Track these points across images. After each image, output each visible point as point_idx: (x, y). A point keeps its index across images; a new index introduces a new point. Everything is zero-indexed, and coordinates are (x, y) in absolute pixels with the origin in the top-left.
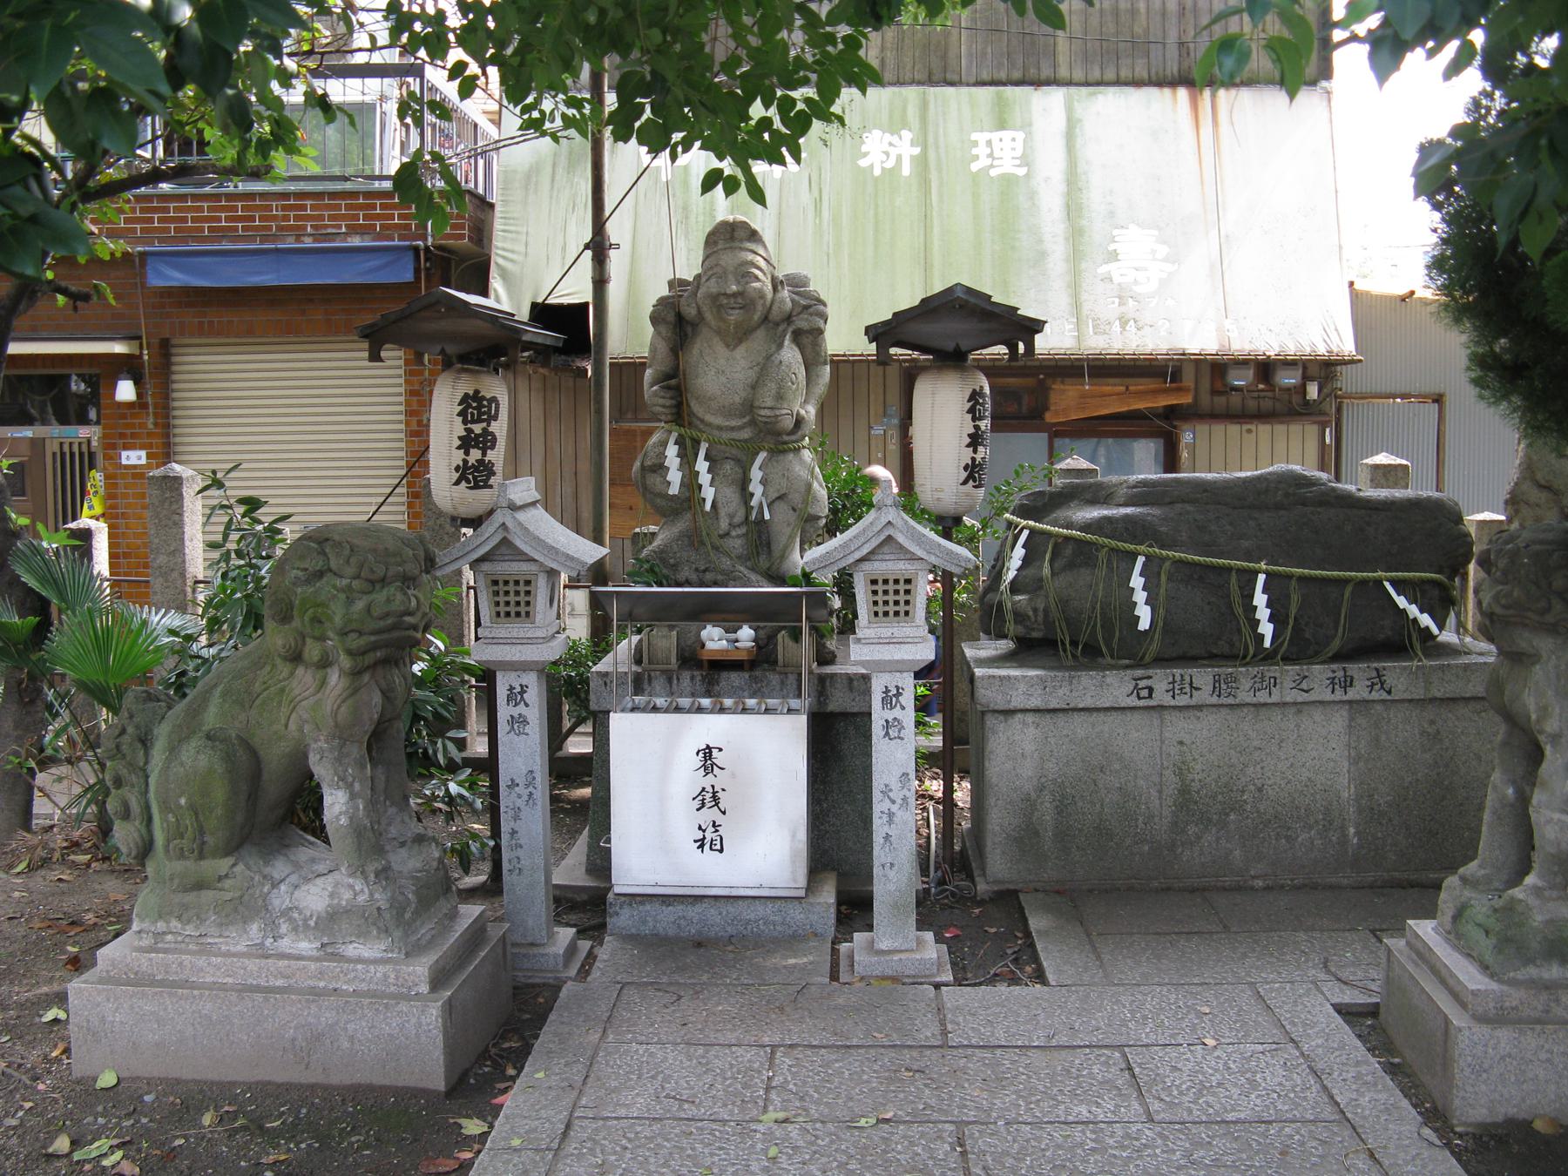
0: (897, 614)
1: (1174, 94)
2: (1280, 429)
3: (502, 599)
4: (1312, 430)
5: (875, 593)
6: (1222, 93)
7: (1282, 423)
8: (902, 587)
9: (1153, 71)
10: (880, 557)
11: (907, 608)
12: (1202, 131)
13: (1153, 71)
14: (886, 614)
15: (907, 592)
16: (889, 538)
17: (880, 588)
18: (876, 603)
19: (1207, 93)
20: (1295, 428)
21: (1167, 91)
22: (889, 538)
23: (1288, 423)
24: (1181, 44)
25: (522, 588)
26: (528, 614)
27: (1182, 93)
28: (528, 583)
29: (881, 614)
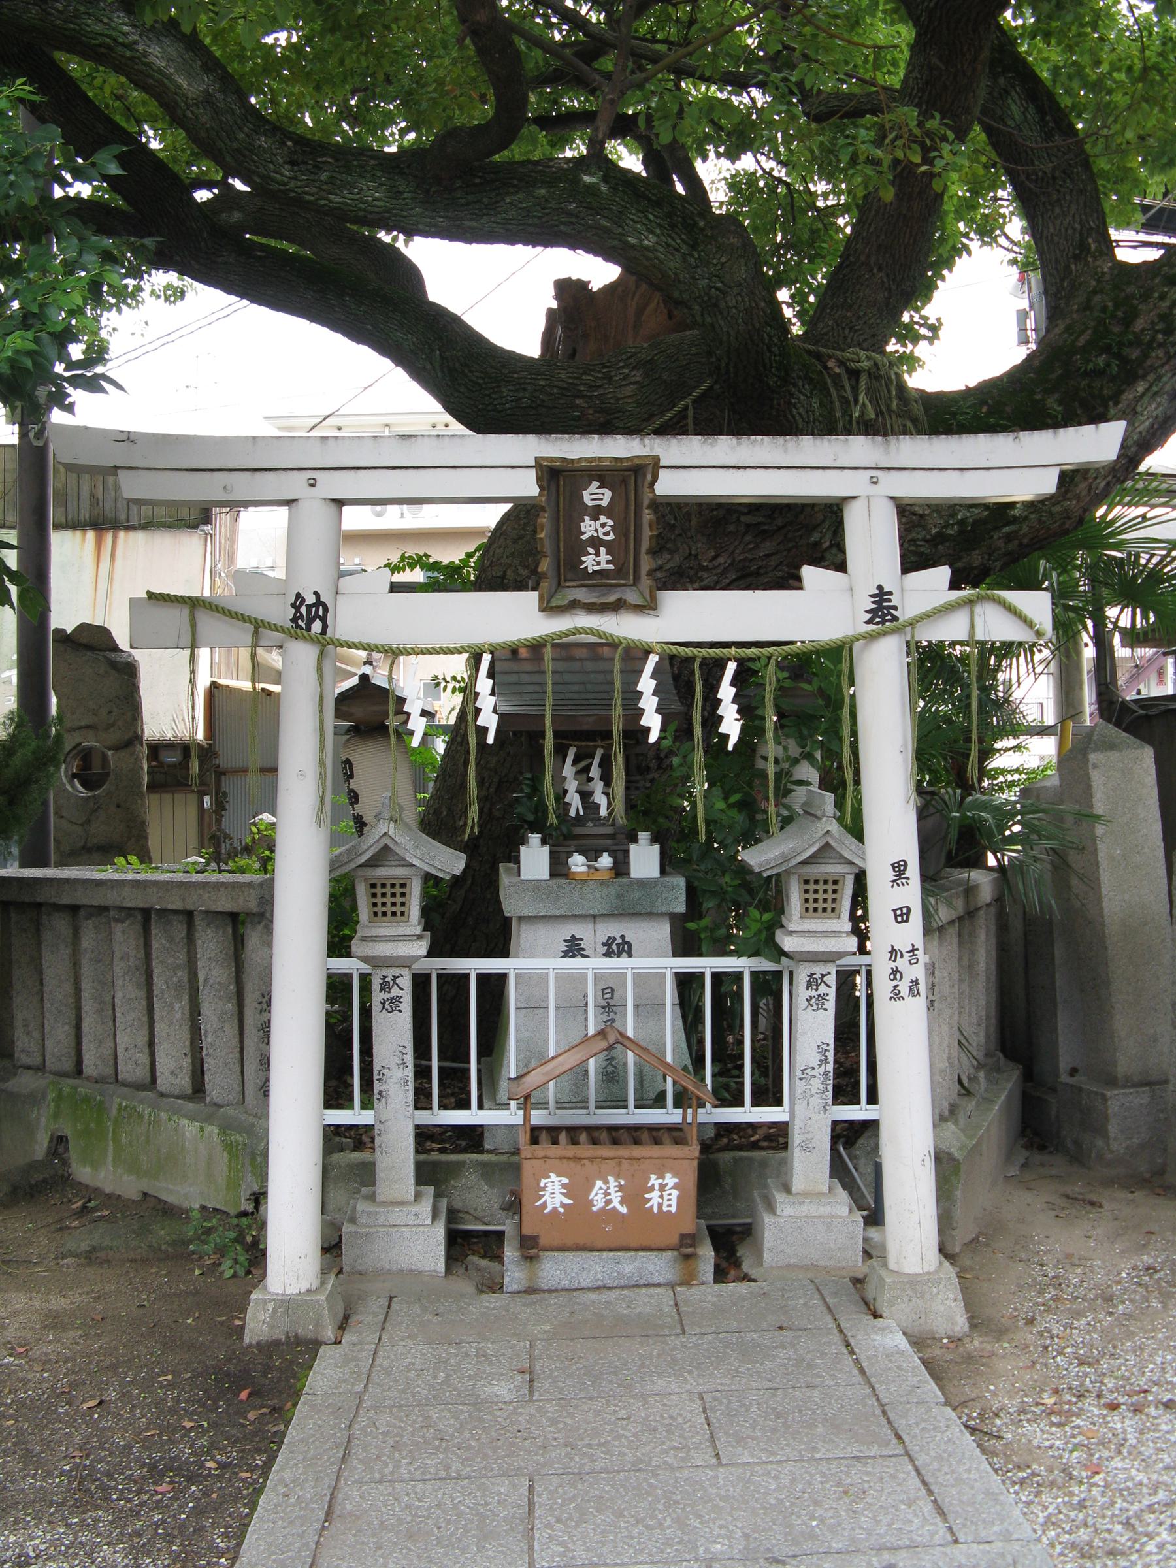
0: (394, 914)
1: (84, 535)
2: (167, 797)
3: (811, 896)
4: (193, 799)
5: (374, 895)
6: (122, 534)
7: (167, 792)
8: (398, 890)
9: (70, 517)
10: (820, 861)
11: (403, 909)
12: (101, 565)
13: (70, 517)
14: (815, 910)
15: (403, 895)
16: (827, 844)
17: (379, 891)
18: (375, 905)
19: (109, 536)
20: (179, 797)
21: (78, 533)
22: (827, 844)
23: (173, 792)
24: (92, 496)
25: (398, 890)
26: (403, 914)
27: (91, 535)
28: (403, 885)
29: (379, 914)
